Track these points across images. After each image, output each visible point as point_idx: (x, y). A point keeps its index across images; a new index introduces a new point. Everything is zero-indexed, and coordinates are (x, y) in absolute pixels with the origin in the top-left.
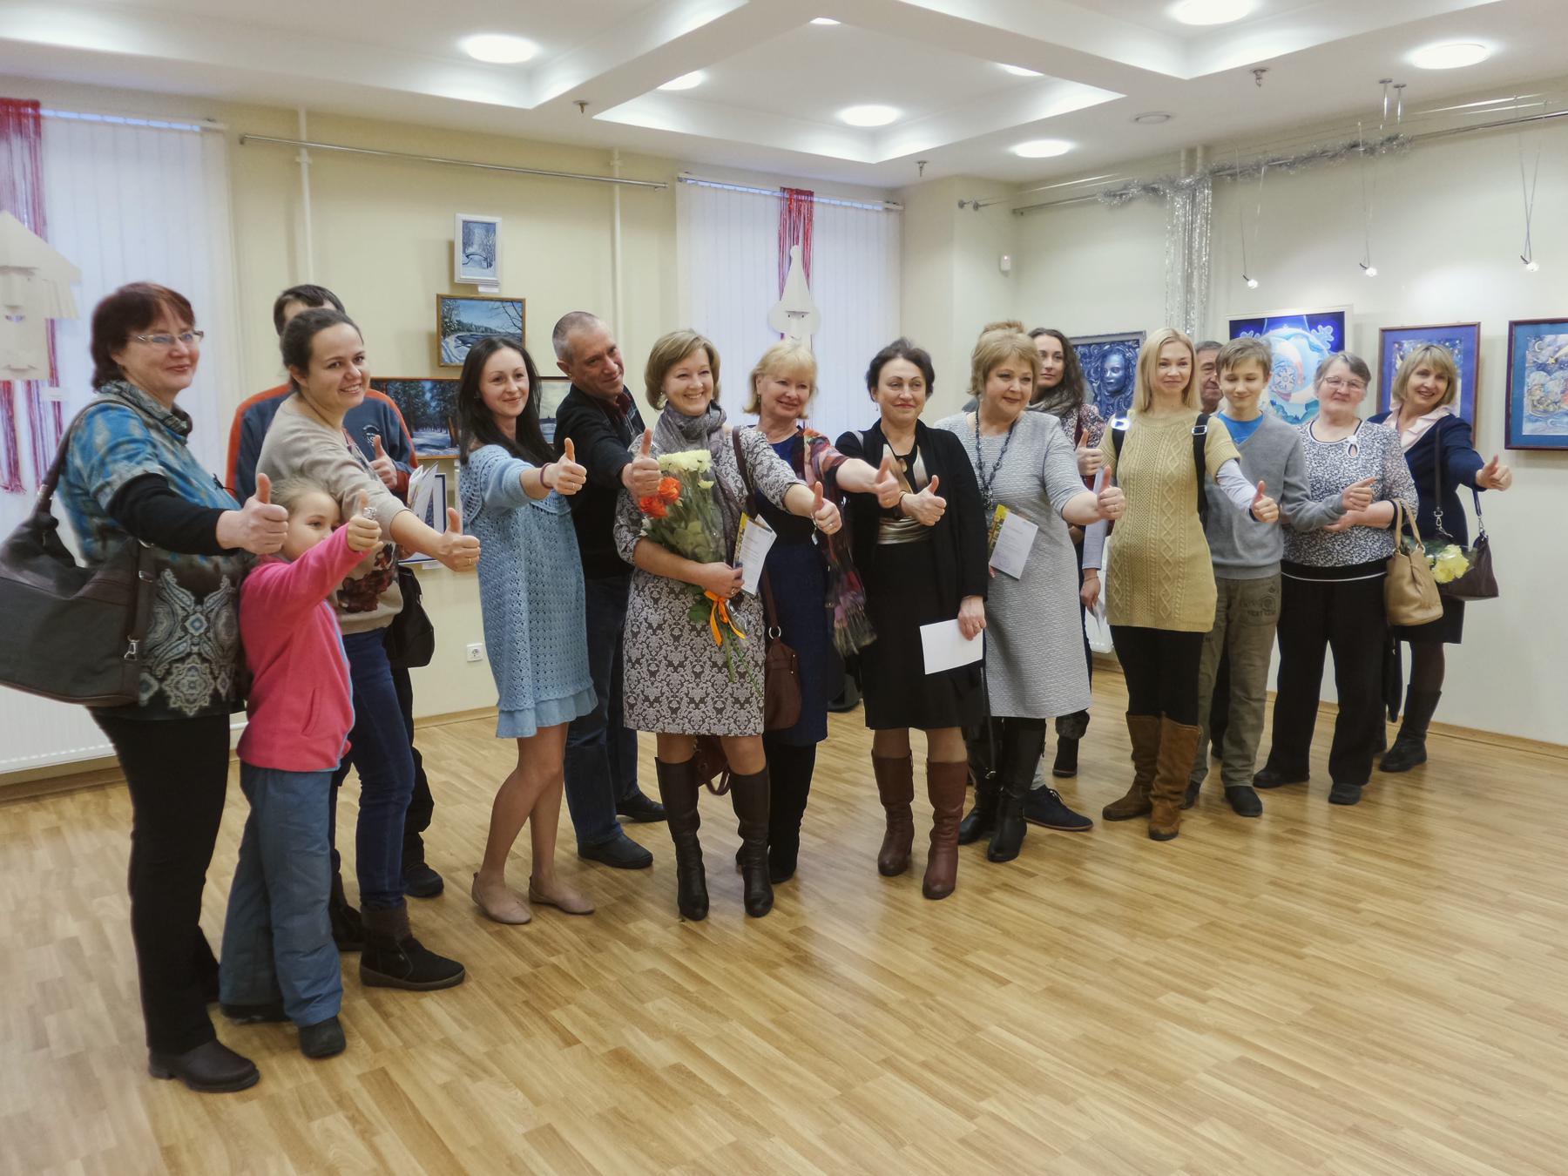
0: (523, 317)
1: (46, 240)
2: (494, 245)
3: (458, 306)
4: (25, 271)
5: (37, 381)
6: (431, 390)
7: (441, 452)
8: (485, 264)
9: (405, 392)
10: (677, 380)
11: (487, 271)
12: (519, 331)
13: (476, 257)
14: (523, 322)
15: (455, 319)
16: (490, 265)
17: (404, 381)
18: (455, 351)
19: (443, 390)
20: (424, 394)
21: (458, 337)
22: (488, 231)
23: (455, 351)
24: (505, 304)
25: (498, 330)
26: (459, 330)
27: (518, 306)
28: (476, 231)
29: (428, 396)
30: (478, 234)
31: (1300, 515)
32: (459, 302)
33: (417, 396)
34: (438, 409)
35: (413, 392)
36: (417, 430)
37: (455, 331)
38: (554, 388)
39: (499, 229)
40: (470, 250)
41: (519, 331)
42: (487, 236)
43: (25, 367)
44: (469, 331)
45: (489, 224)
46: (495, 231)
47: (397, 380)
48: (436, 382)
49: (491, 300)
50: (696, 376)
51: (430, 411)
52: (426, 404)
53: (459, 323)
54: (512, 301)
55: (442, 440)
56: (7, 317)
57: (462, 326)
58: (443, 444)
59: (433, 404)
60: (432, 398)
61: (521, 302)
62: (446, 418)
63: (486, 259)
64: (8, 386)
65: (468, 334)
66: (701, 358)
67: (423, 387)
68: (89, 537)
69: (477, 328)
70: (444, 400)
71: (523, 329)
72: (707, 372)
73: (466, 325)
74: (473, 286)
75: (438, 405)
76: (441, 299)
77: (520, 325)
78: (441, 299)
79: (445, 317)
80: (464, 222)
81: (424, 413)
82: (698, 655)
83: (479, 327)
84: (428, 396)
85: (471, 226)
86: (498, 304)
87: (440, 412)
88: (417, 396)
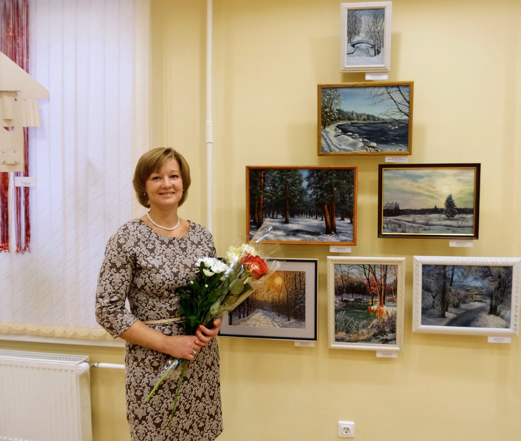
0: (410, 103)
1: (27, 71)
2: (383, 32)
3: (339, 95)
4: (14, 93)
5: (20, 172)
6: (308, 178)
7: (316, 238)
8: (372, 52)
9: (282, 180)
10: (152, 182)
11: (375, 59)
12: (406, 117)
13: (363, 46)
14: (410, 107)
15: (335, 108)
16: (378, 52)
17: (282, 170)
18: (335, 140)
19: (321, 179)
20: (301, 182)
21: (338, 127)
22: (376, 17)
23: (335, 140)
24: (390, 90)
25: (381, 117)
26: (339, 119)
27: (404, 90)
28: (363, 18)
29: (305, 184)
30: (365, 21)
31: (271, 320)
32: (340, 91)
33: (293, 184)
34: (314, 197)
35: (290, 180)
36: (292, 216)
37: (335, 120)
38: (444, 176)
39: (388, 13)
40: (356, 39)
41: (406, 117)
42: (375, 23)
43: (14, 163)
44: (349, 119)
45: (378, 9)
46: (383, 16)
47: (274, 169)
48: (313, 171)
49: (375, 86)
50: (166, 178)
51: (307, 198)
52: (303, 192)
53: (340, 111)
54: (398, 86)
55: (317, 227)
56: (7, 128)
57: (342, 116)
58: (318, 230)
59: (310, 192)
60: (309, 186)
61: (409, 86)
62: (322, 205)
63: (373, 46)
64: (5, 175)
65: (349, 122)
66: (172, 166)
67: (301, 176)
68: (341, 311)
69: (359, 116)
70: (321, 188)
71: (410, 115)
72: (177, 176)
73: (346, 113)
74: (361, 75)
75: (315, 193)
76: (323, 90)
77: (407, 111)
78: (323, 90)
79: (325, 107)
80: (349, 10)
81: (300, 201)
82: (157, 409)
83: (361, 115)
84: (305, 184)
85: (358, 13)
86: (383, 90)
87: (317, 200)
88: (293, 184)
